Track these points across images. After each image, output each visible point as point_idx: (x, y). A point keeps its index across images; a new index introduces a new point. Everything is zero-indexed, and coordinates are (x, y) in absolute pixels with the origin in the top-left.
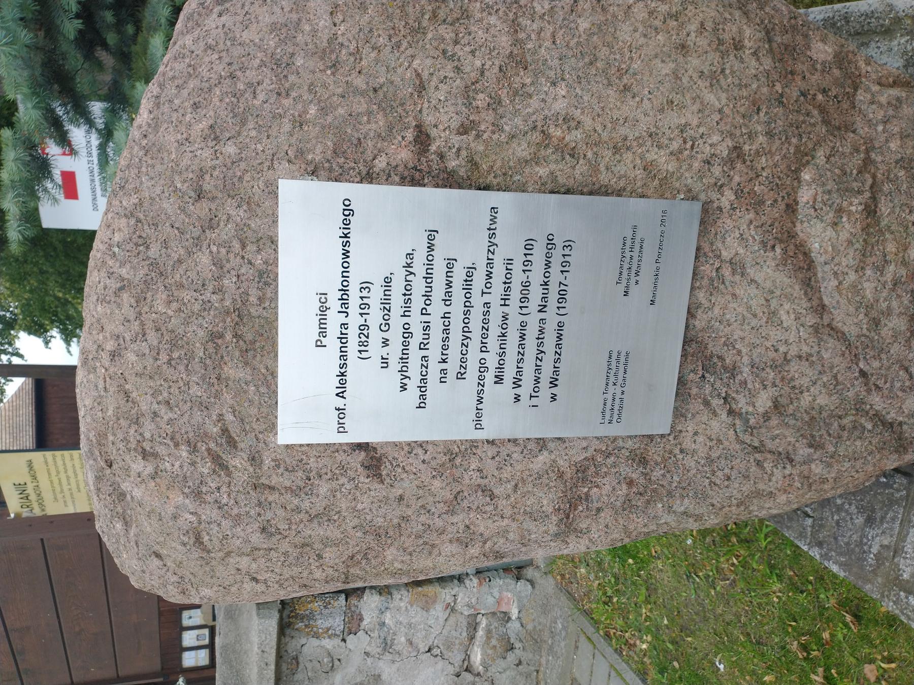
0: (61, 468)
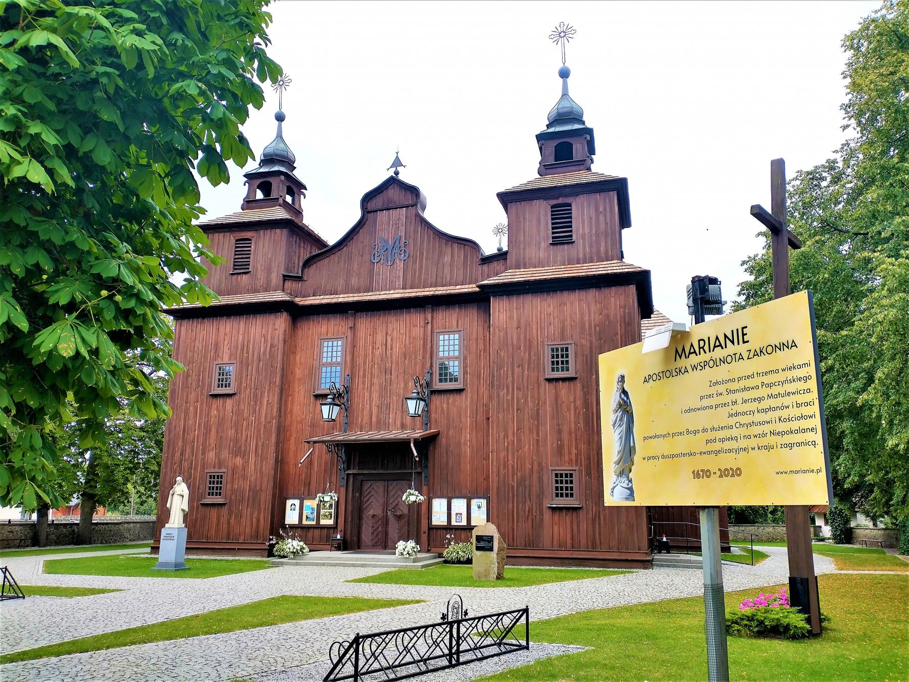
0: (775, 390)
